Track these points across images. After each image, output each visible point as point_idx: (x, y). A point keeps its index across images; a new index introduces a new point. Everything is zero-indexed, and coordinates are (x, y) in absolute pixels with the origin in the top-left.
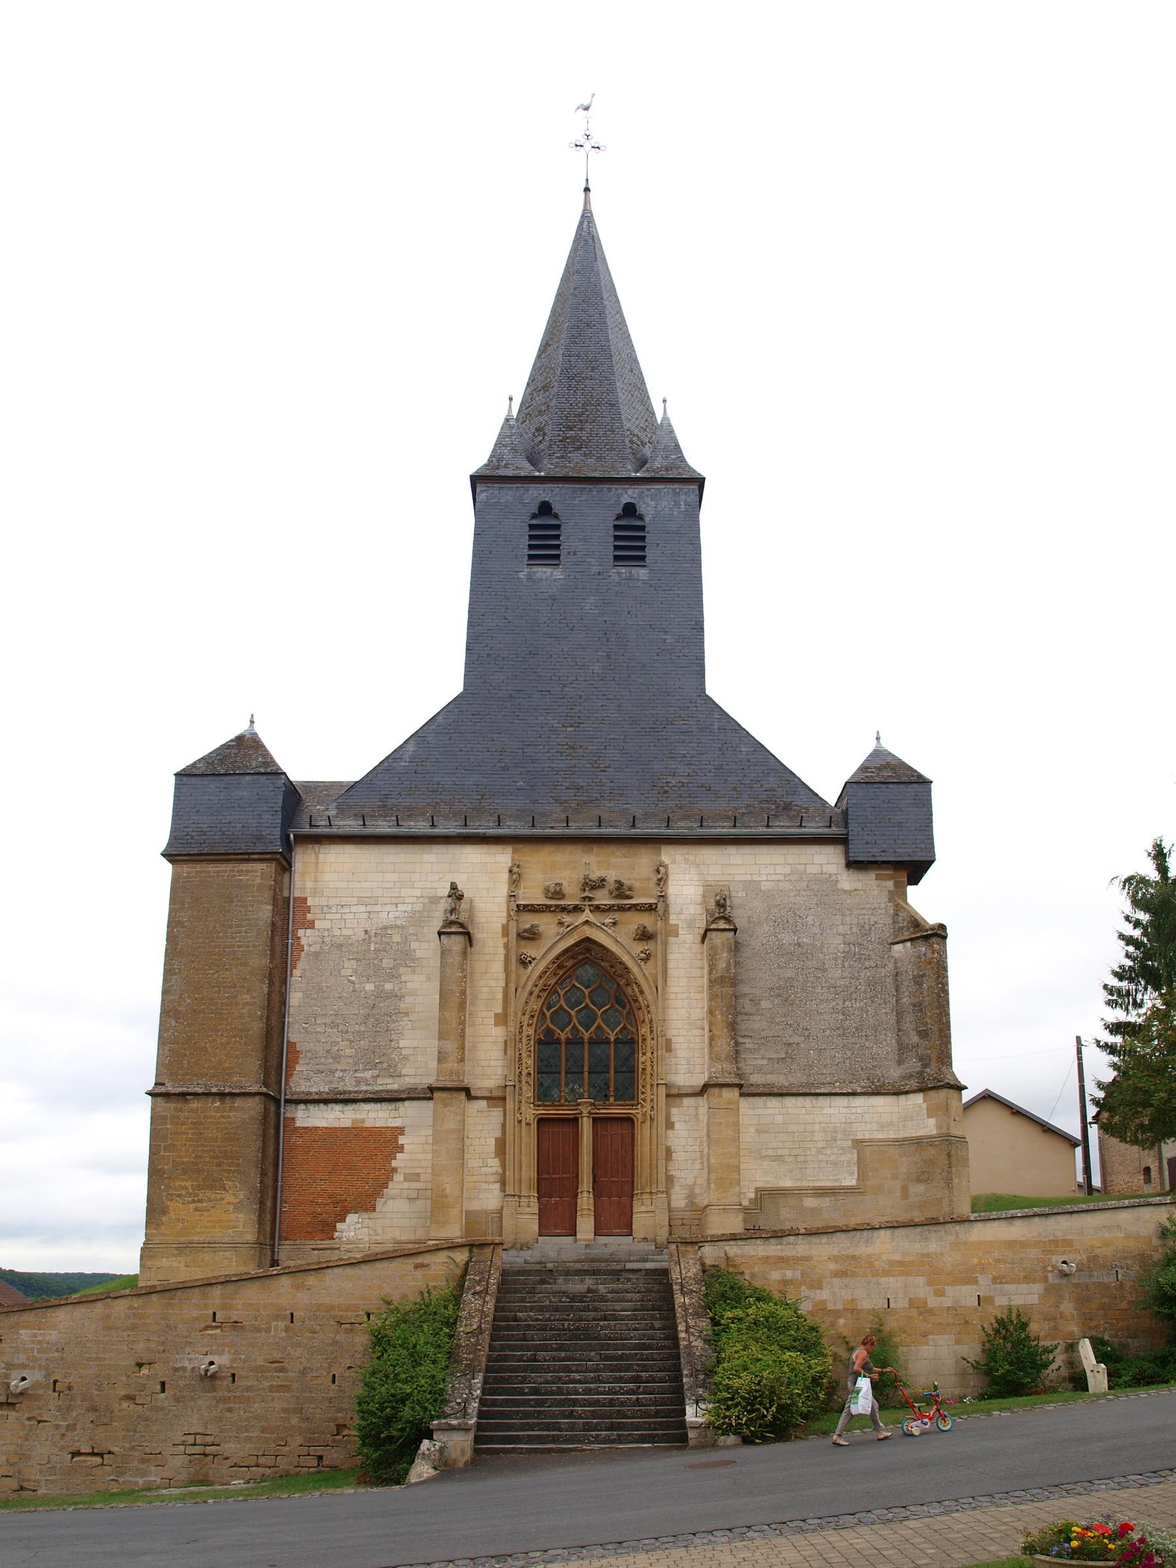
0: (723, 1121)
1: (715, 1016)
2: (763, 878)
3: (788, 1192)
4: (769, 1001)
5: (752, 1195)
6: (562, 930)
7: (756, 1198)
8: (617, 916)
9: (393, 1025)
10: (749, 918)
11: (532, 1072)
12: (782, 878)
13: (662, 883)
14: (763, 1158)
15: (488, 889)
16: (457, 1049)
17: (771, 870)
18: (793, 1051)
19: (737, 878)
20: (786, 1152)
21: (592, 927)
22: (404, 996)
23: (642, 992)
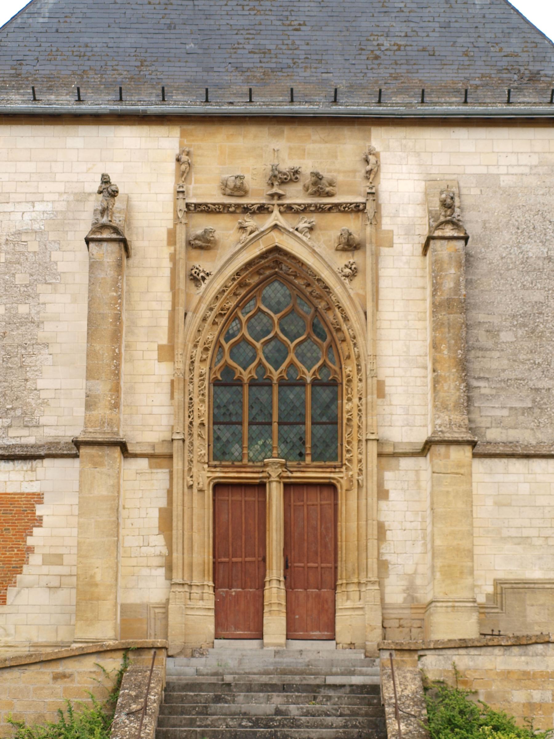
0: (450, 489)
1: (440, 352)
2: (503, 170)
3: (536, 586)
4: (511, 333)
5: (490, 589)
6: (245, 237)
7: (495, 594)
8: (315, 219)
9: (28, 360)
10: (485, 222)
11: (206, 422)
12: (527, 170)
13: (372, 176)
14: (504, 539)
15: (149, 183)
16: (110, 390)
17: (513, 160)
18: (542, 399)
19: (469, 170)
20: (533, 533)
21: (282, 233)
22: (43, 322)
23: (346, 319)
